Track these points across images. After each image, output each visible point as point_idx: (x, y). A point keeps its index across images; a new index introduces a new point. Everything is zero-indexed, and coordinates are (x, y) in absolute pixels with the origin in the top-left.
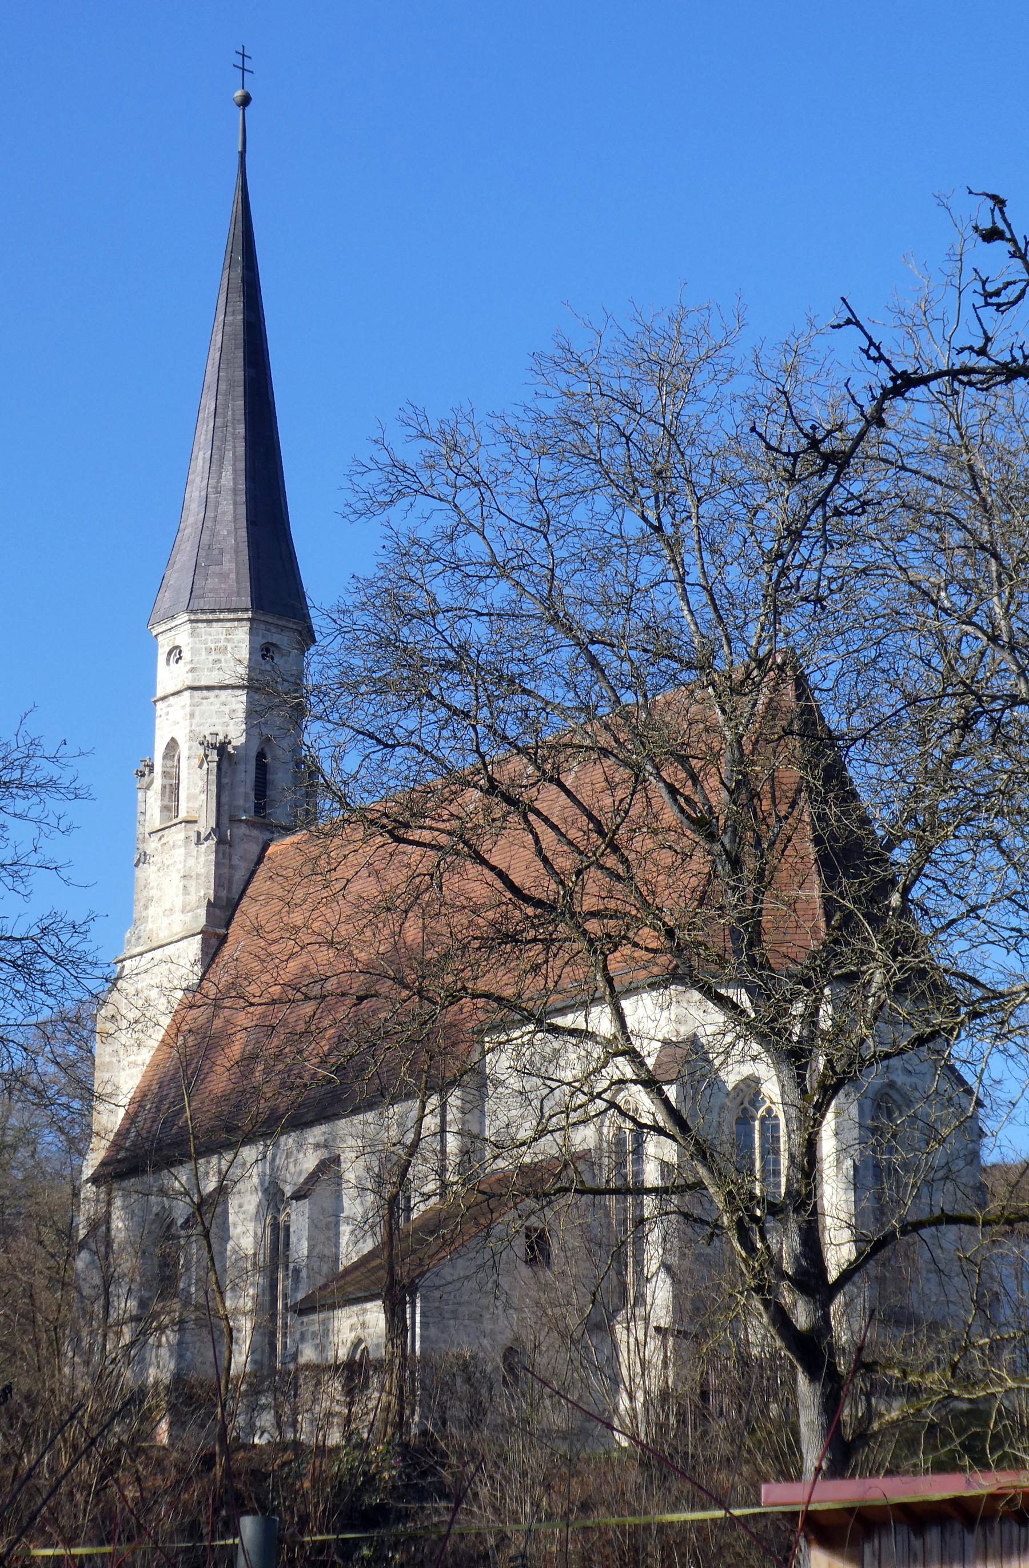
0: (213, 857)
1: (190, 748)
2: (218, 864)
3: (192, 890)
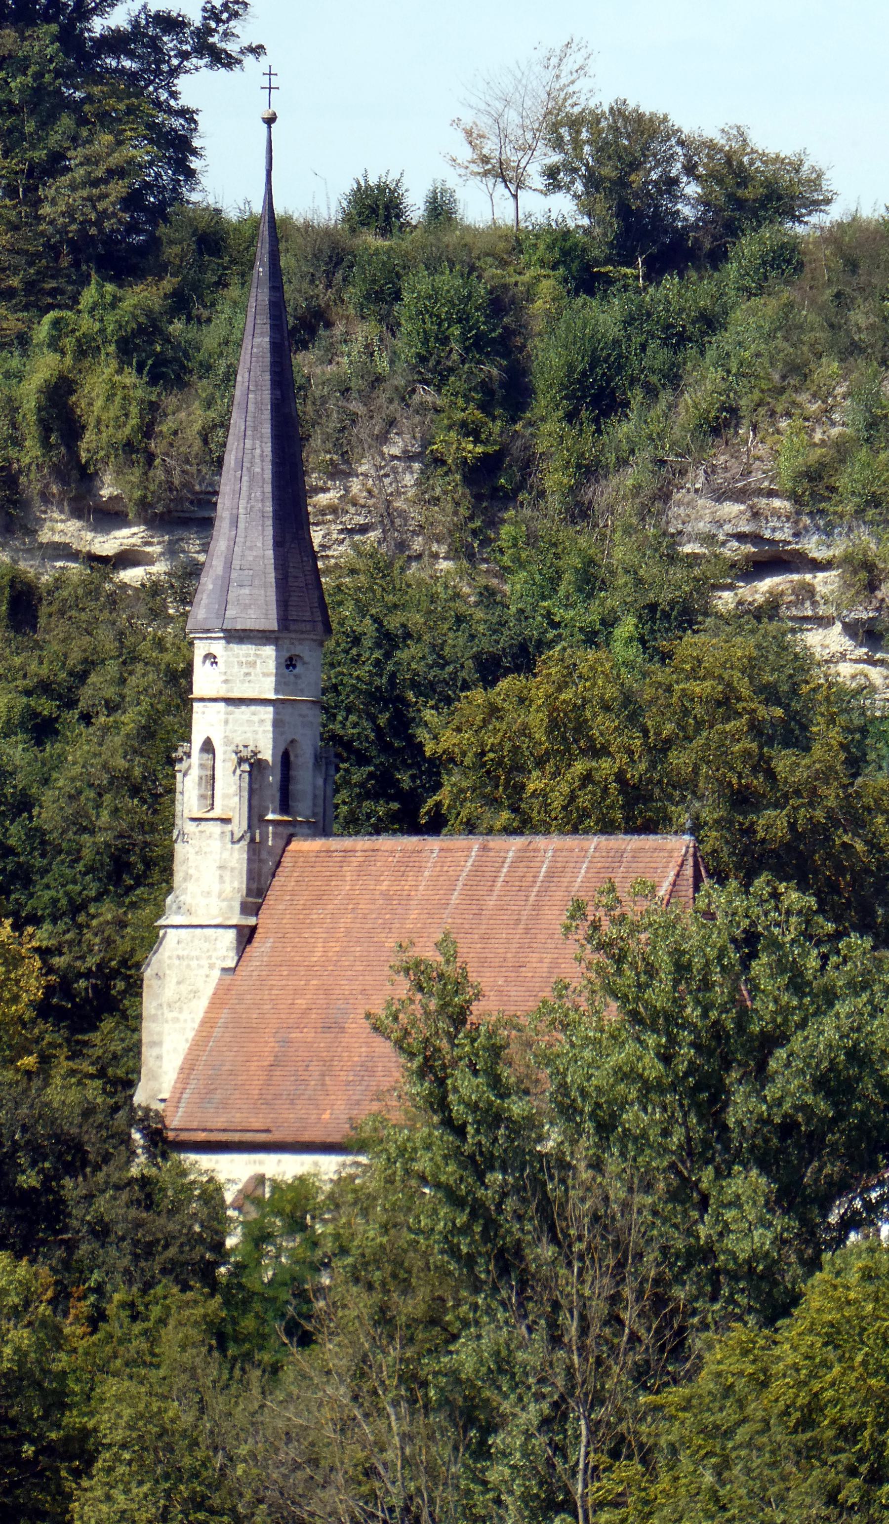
0: (245, 856)
1: (225, 753)
2: (249, 860)
3: (227, 878)
